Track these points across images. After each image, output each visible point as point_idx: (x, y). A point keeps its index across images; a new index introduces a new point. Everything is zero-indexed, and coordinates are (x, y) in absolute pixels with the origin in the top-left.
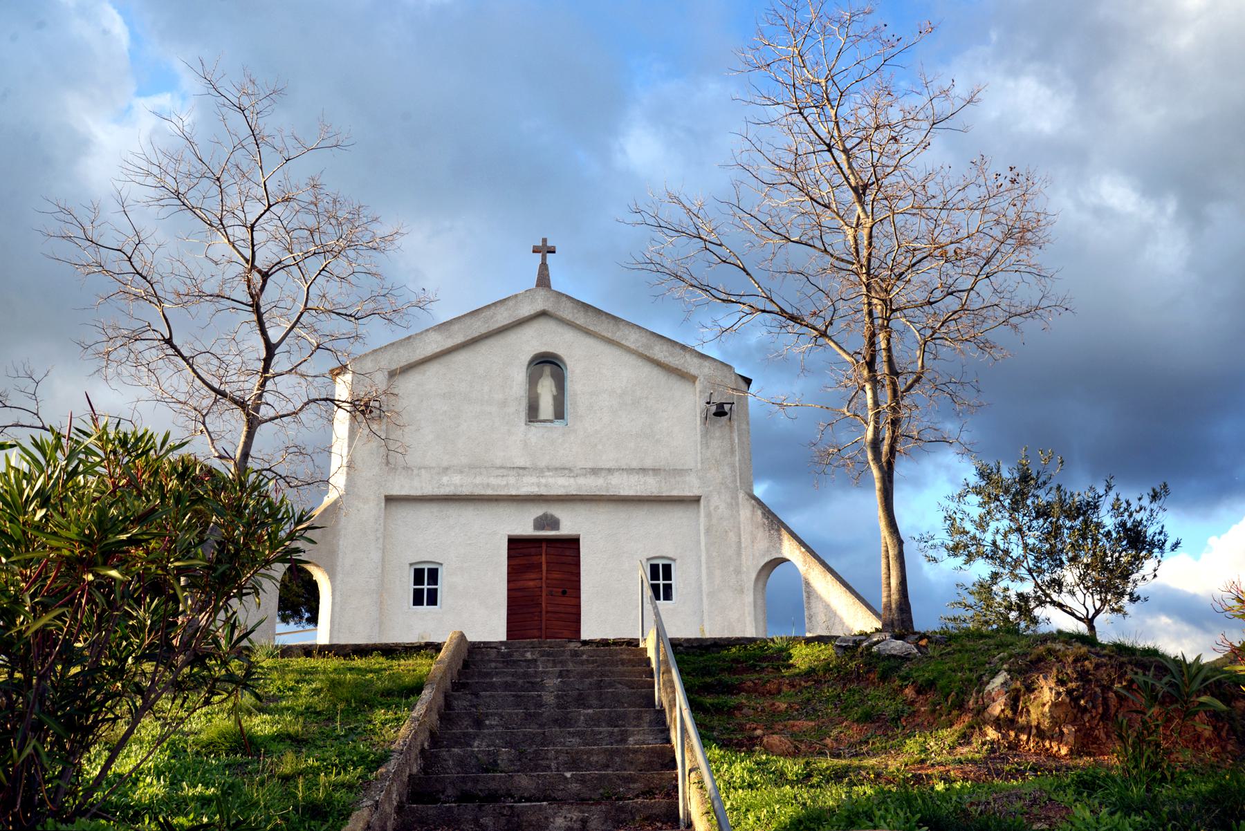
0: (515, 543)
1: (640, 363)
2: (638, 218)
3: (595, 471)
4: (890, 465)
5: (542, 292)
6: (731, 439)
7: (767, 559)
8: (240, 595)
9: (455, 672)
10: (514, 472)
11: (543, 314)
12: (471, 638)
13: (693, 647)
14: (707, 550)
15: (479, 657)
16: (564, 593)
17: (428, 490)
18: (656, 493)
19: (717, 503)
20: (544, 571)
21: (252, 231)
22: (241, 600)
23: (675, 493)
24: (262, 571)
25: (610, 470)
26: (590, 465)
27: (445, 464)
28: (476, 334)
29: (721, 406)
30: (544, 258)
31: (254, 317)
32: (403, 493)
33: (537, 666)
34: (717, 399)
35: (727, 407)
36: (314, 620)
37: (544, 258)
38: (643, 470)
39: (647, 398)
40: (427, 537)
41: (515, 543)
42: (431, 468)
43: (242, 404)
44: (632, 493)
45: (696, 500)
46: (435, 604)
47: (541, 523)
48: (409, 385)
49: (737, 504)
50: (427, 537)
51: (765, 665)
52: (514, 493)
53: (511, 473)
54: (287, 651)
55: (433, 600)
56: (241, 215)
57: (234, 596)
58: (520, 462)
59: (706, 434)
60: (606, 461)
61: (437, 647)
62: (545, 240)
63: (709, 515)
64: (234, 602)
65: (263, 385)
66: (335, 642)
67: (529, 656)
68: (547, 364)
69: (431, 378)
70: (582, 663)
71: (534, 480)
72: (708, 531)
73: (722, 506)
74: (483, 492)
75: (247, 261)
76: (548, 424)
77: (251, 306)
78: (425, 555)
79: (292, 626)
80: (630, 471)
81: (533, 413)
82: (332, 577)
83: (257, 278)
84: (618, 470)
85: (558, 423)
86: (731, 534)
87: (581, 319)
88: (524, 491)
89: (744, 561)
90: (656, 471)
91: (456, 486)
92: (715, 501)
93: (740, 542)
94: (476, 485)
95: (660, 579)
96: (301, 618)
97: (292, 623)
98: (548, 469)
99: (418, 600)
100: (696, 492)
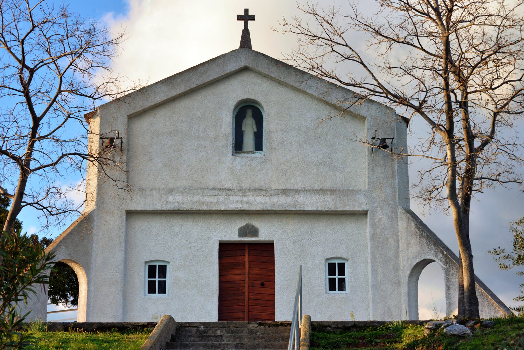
0: (225, 248)
1: (321, 106)
2: (287, 28)
3: (285, 192)
4: (467, 199)
5: (245, 51)
6: (392, 167)
7: (418, 260)
8: (17, 300)
9: (164, 343)
10: (223, 193)
11: (245, 69)
12: (178, 319)
13: (338, 328)
14: (372, 253)
15: (184, 333)
16: (263, 285)
17: (158, 206)
18: (332, 208)
19: (381, 215)
20: (246, 266)
21: (23, 44)
22: (16, 302)
23: (347, 208)
24: (29, 287)
25: (297, 191)
26: (281, 187)
27: (171, 186)
28: (194, 86)
29: (383, 140)
30: (246, 25)
31: (24, 99)
32: (139, 209)
33: (222, 340)
34: (381, 135)
35: (388, 142)
36: (75, 302)
37: (246, 25)
38: (323, 191)
39: (327, 134)
40: (158, 242)
41: (225, 248)
42: (159, 189)
43: (18, 160)
44: (314, 209)
45: (364, 214)
46: (165, 292)
47: (243, 232)
48: (143, 125)
49: (396, 217)
50: (158, 242)
51: (379, 341)
52: (223, 208)
53: (220, 193)
54: (53, 327)
55: (163, 289)
56: (16, 33)
57: (13, 300)
58: (228, 184)
59: (372, 162)
60: (294, 183)
61: (152, 325)
62: (246, 11)
63: (373, 226)
64: (13, 303)
65: (31, 147)
66: (91, 320)
67: (219, 333)
68: (248, 112)
69: (160, 121)
70: (254, 338)
71: (238, 198)
72: (373, 238)
73: (385, 219)
74: (199, 208)
75: (20, 62)
76: (250, 155)
77: (23, 92)
78: (156, 254)
79: (61, 306)
80: (313, 191)
81: (238, 146)
82: (88, 272)
83: (26, 74)
84: (303, 191)
85: (258, 154)
86: (391, 240)
87: (275, 73)
88: (231, 207)
89: (401, 261)
90: (332, 191)
91: (179, 203)
92: (379, 214)
93: (398, 247)
94: (194, 203)
95: (336, 276)
96: (67, 301)
97: (60, 305)
98: (249, 190)
99: (151, 289)
100: (364, 208)
